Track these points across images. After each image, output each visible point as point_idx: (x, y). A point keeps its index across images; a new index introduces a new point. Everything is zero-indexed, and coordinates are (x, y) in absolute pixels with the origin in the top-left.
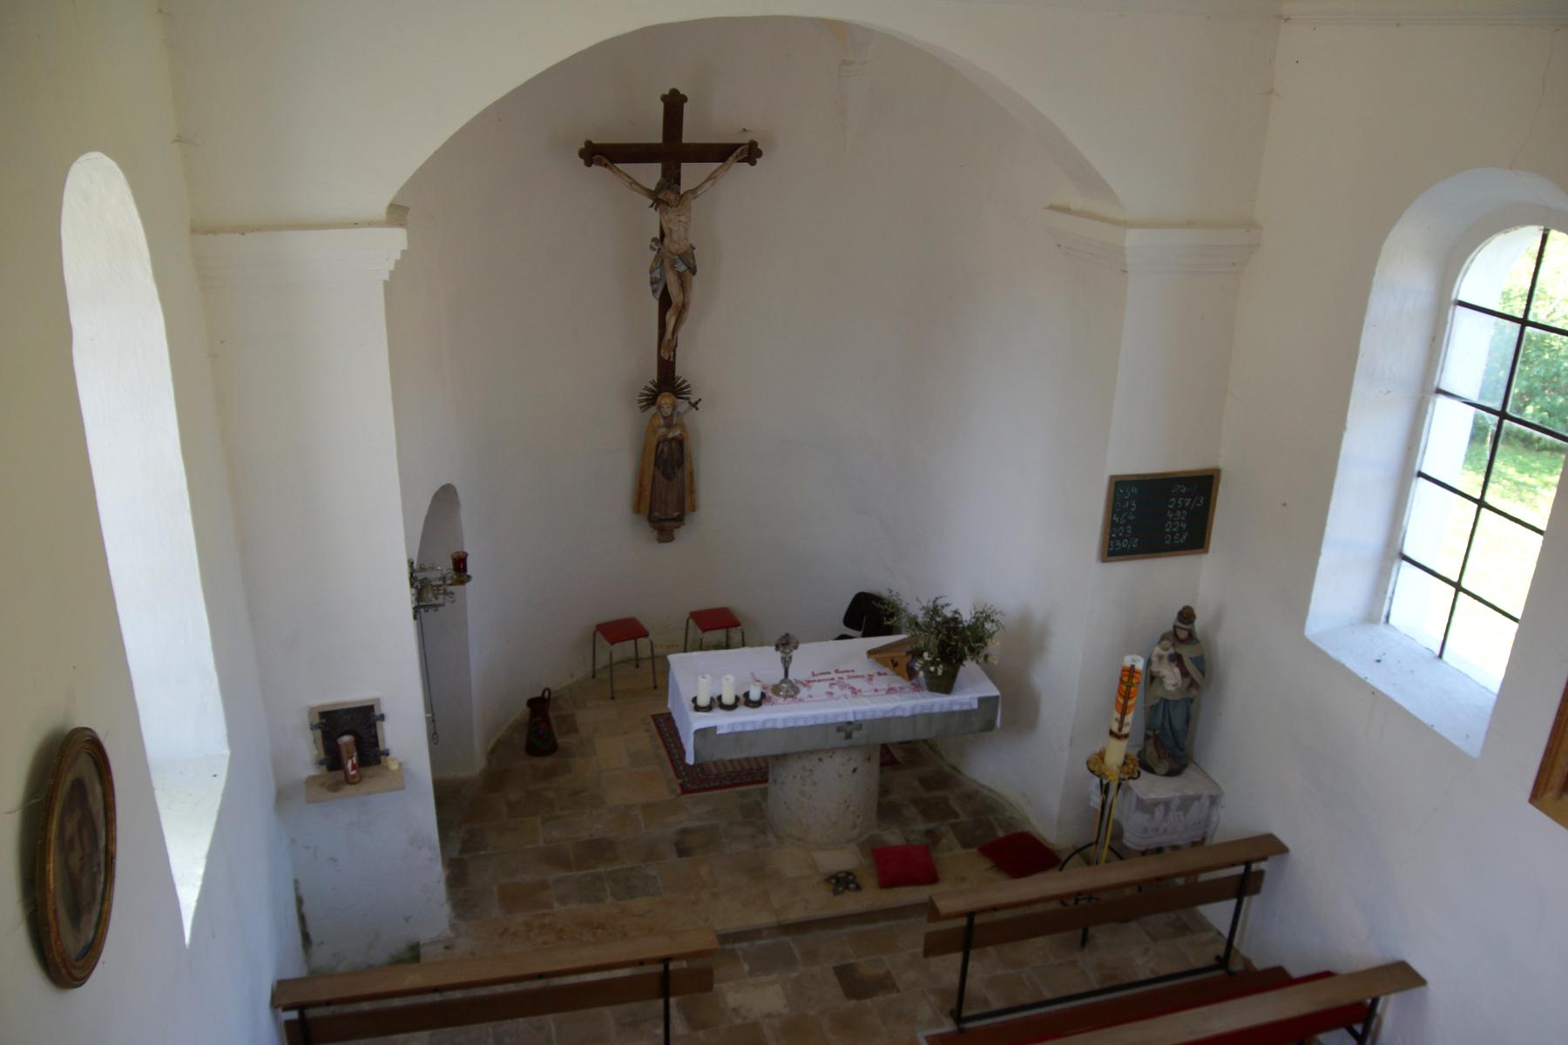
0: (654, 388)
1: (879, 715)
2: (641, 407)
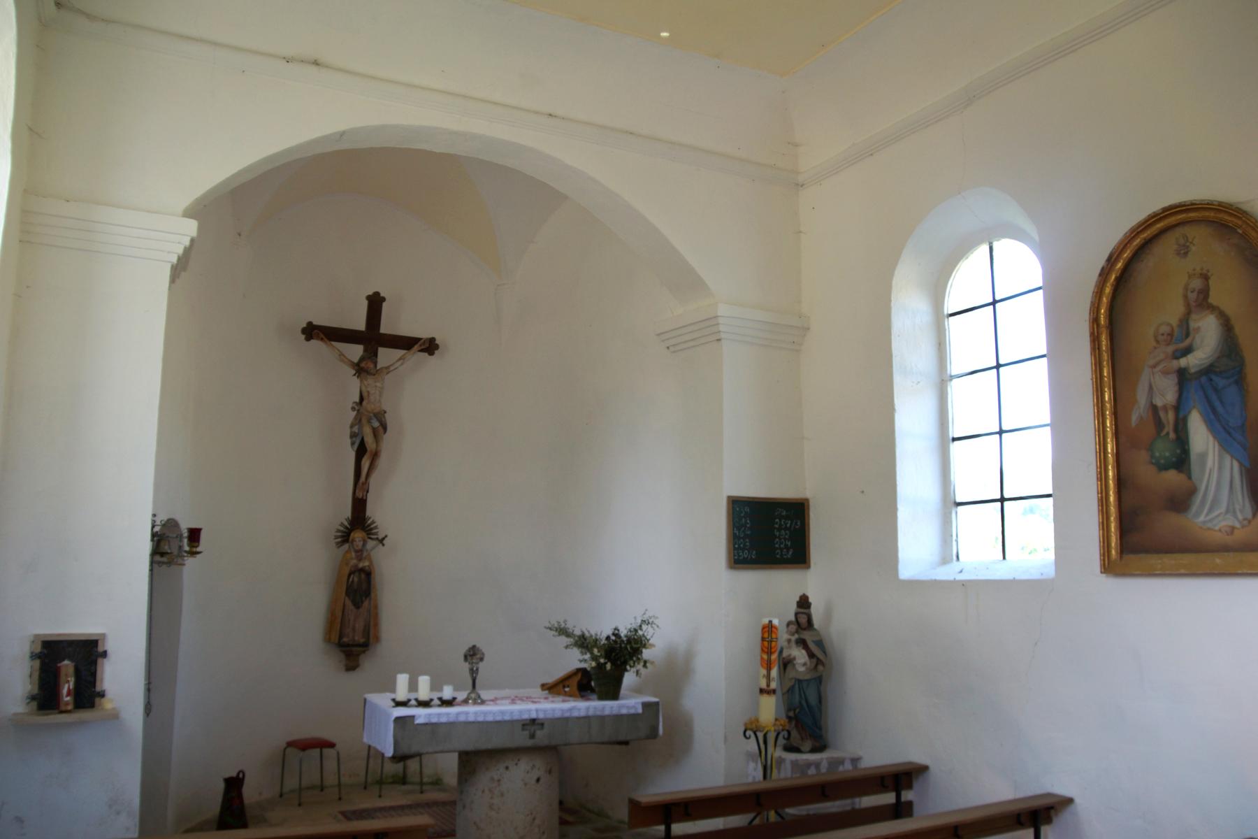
0: (348, 526)
1: (558, 715)
2: (337, 543)
